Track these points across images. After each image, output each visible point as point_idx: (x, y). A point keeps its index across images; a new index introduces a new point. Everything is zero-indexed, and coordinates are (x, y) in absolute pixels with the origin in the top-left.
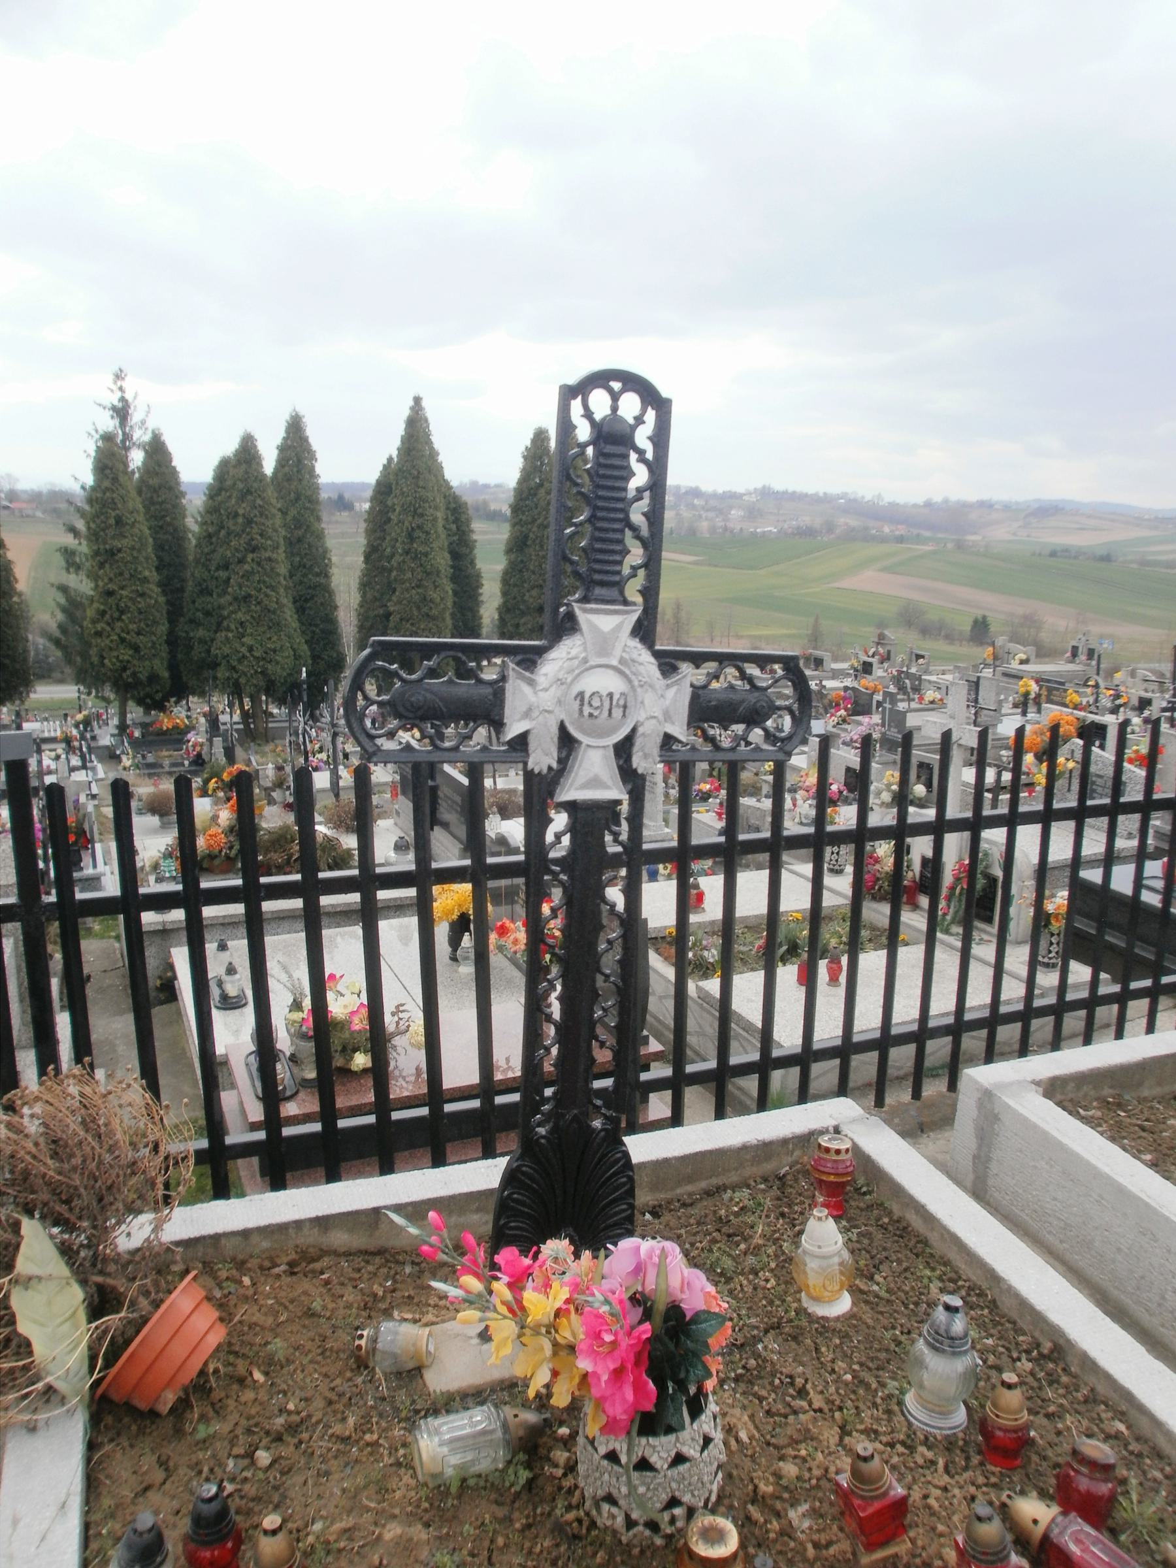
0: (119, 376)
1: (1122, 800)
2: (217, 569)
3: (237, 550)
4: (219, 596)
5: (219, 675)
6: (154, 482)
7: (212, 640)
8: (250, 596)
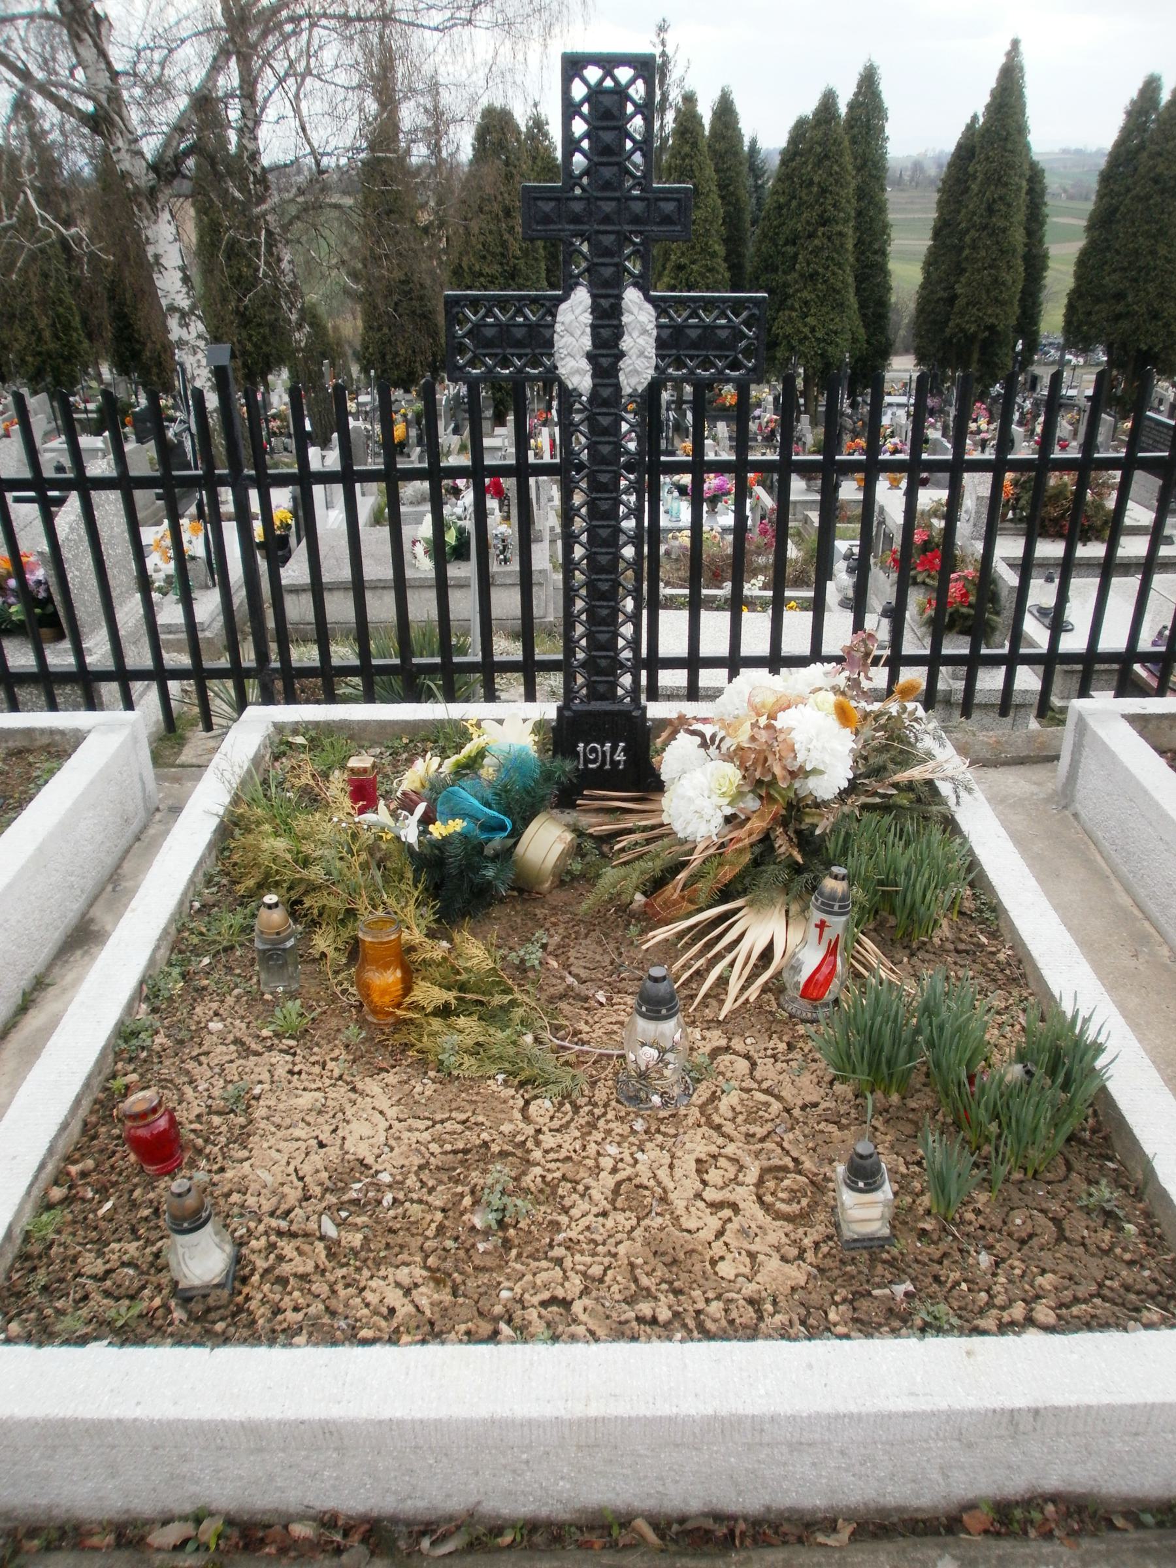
0: (662, 29)
2: (785, 245)
3: (808, 223)
4: (785, 273)
5: (778, 355)
6: (720, 146)
7: (774, 319)
8: (817, 273)
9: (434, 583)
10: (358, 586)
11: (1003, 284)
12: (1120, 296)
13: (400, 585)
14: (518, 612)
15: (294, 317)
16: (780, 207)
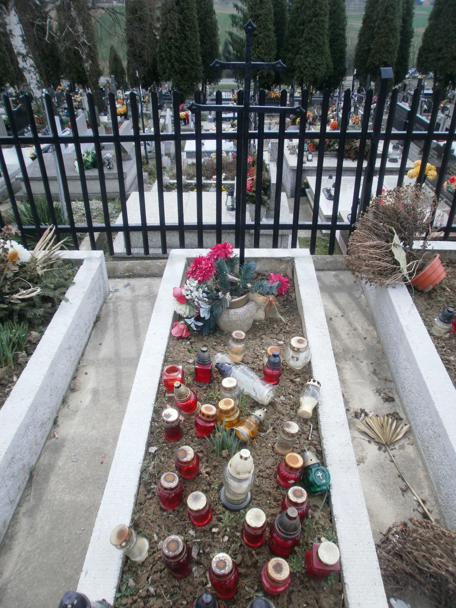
2: (299, 25)
4: (299, 38)
7: (294, 59)
10: (45, 179)
11: (391, 44)
12: (440, 50)
14: (118, 190)
15: (84, 57)
16: (297, 9)
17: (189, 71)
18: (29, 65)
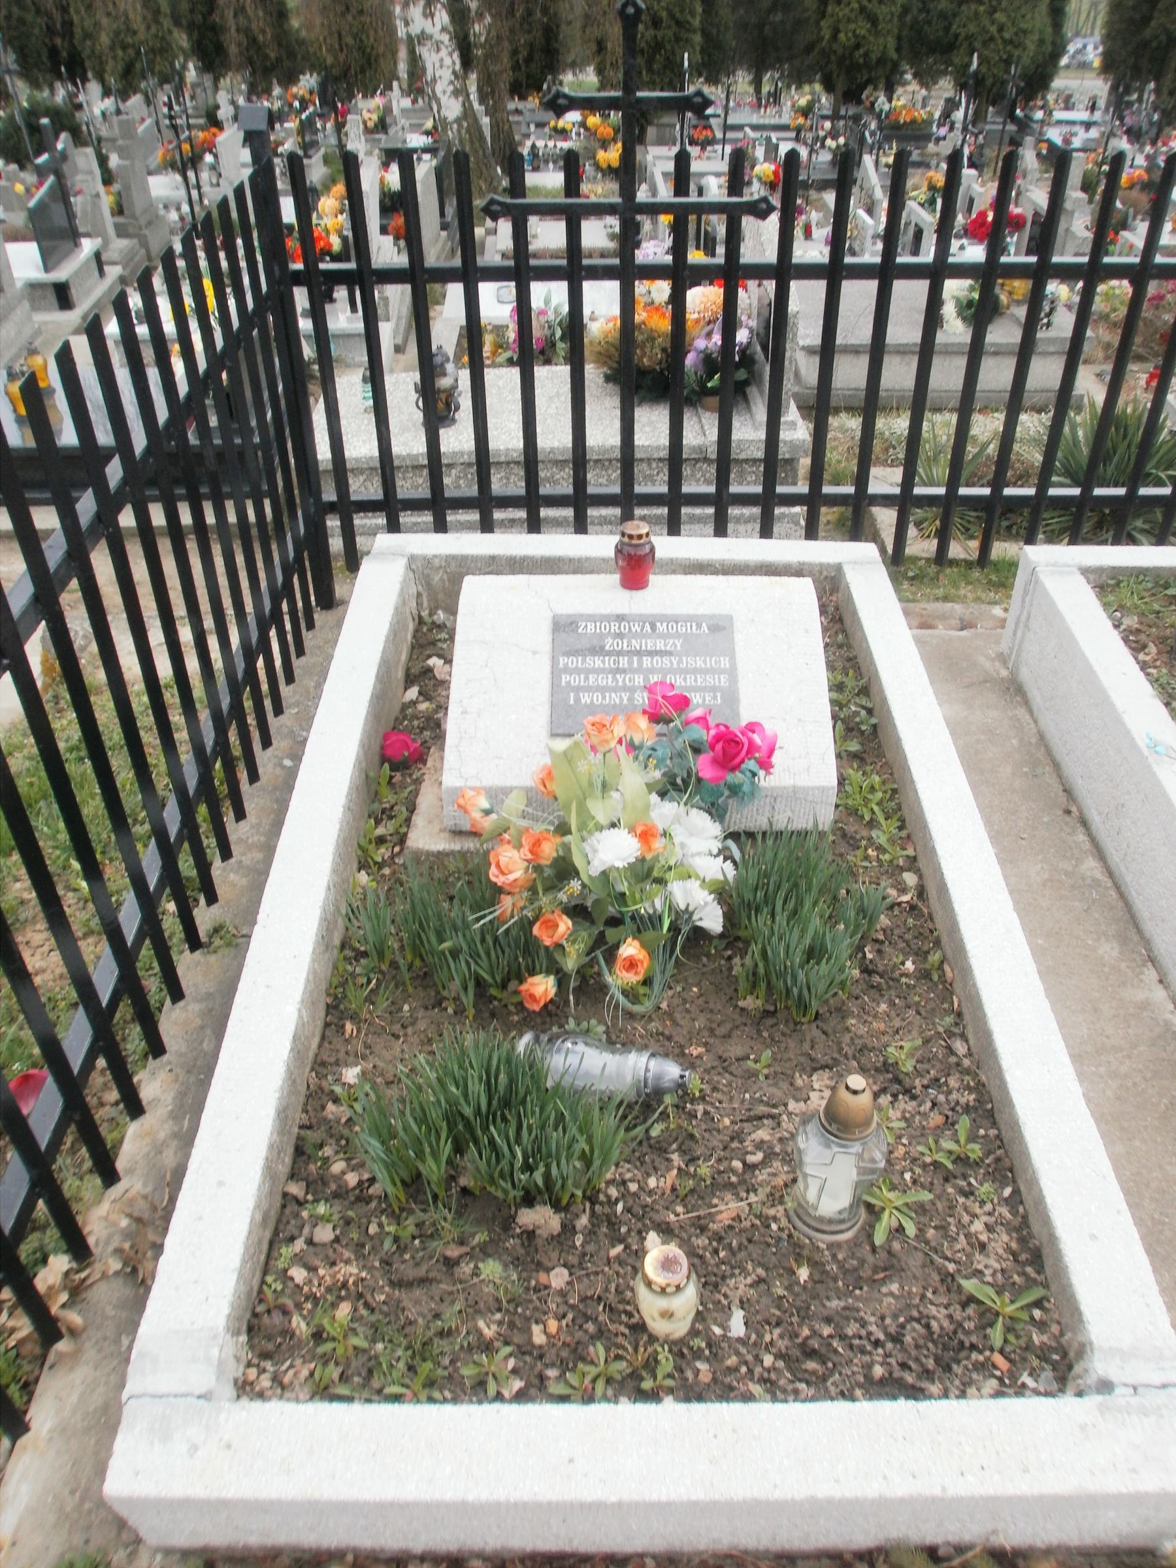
1: (1106, 260)
7: (955, 15)
9: (967, 349)
13: (926, 351)
17: (668, 47)
18: (438, 27)
